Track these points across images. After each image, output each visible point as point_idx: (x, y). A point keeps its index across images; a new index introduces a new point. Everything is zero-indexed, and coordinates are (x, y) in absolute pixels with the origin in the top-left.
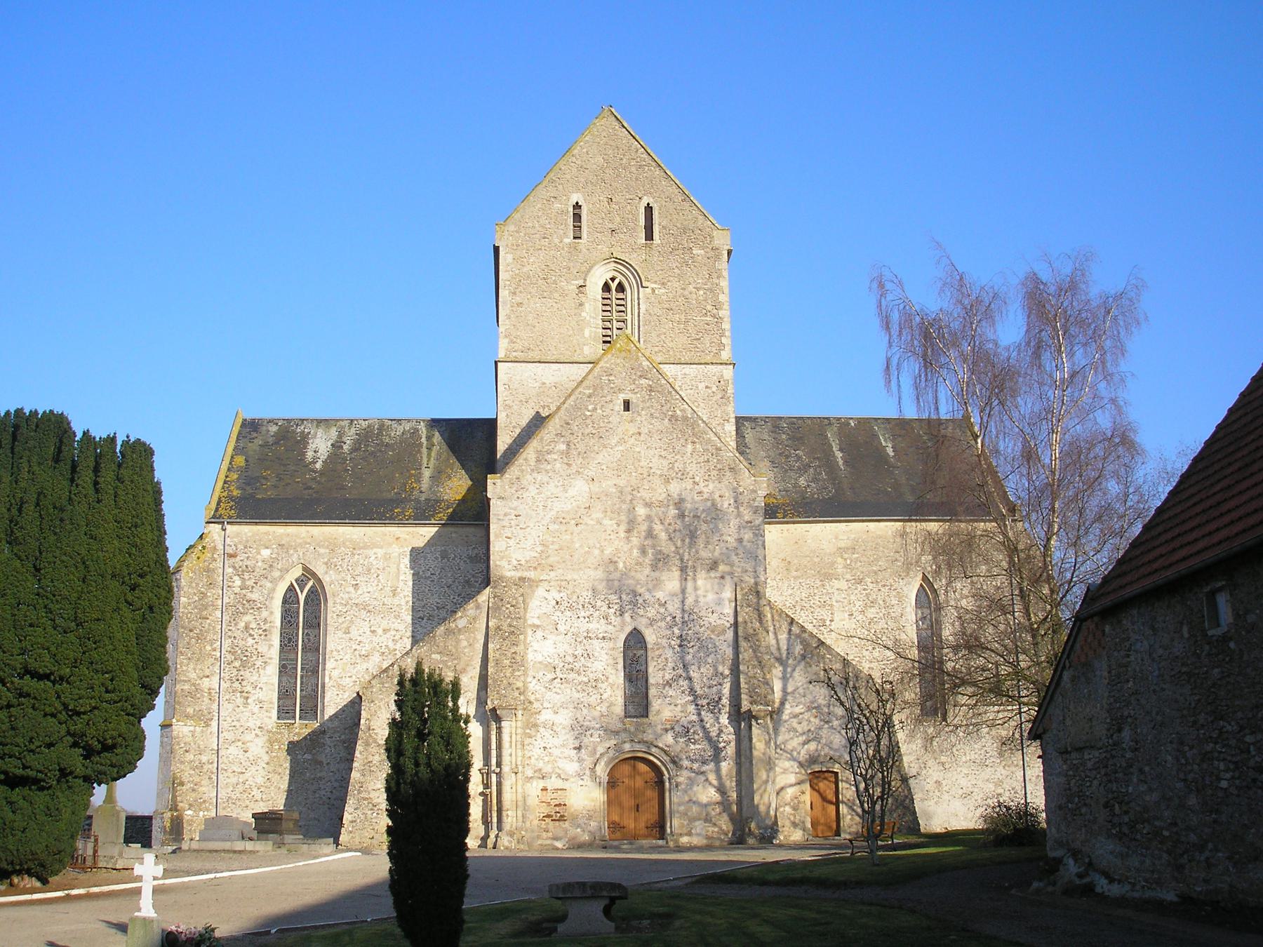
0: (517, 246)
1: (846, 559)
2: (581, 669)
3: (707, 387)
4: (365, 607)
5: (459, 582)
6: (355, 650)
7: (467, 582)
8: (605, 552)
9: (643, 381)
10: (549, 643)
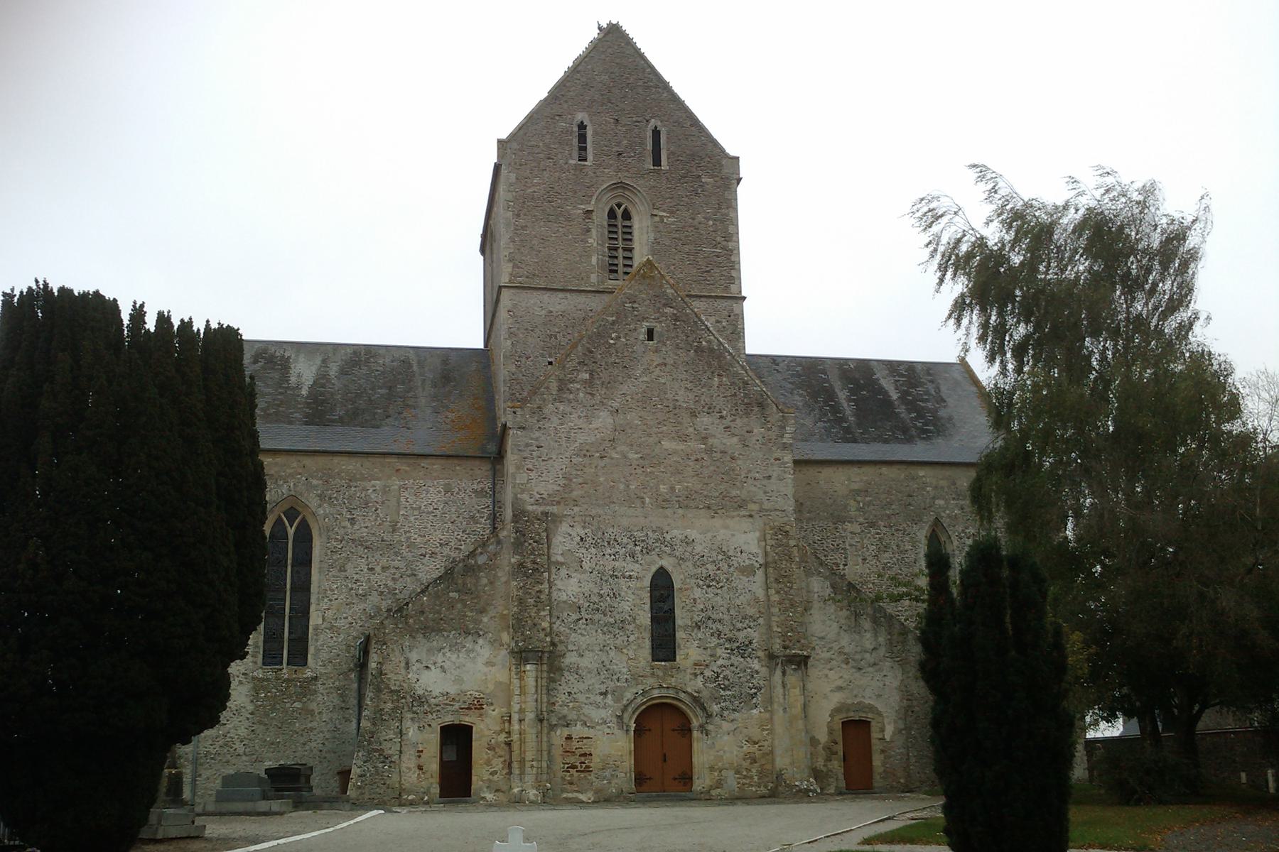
0: (521, 165)
1: (858, 502)
2: (607, 610)
3: (717, 322)
4: (361, 542)
5: (463, 518)
6: (352, 589)
7: (472, 517)
8: (631, 487)
9: (667, 310)
10: (574, 581)
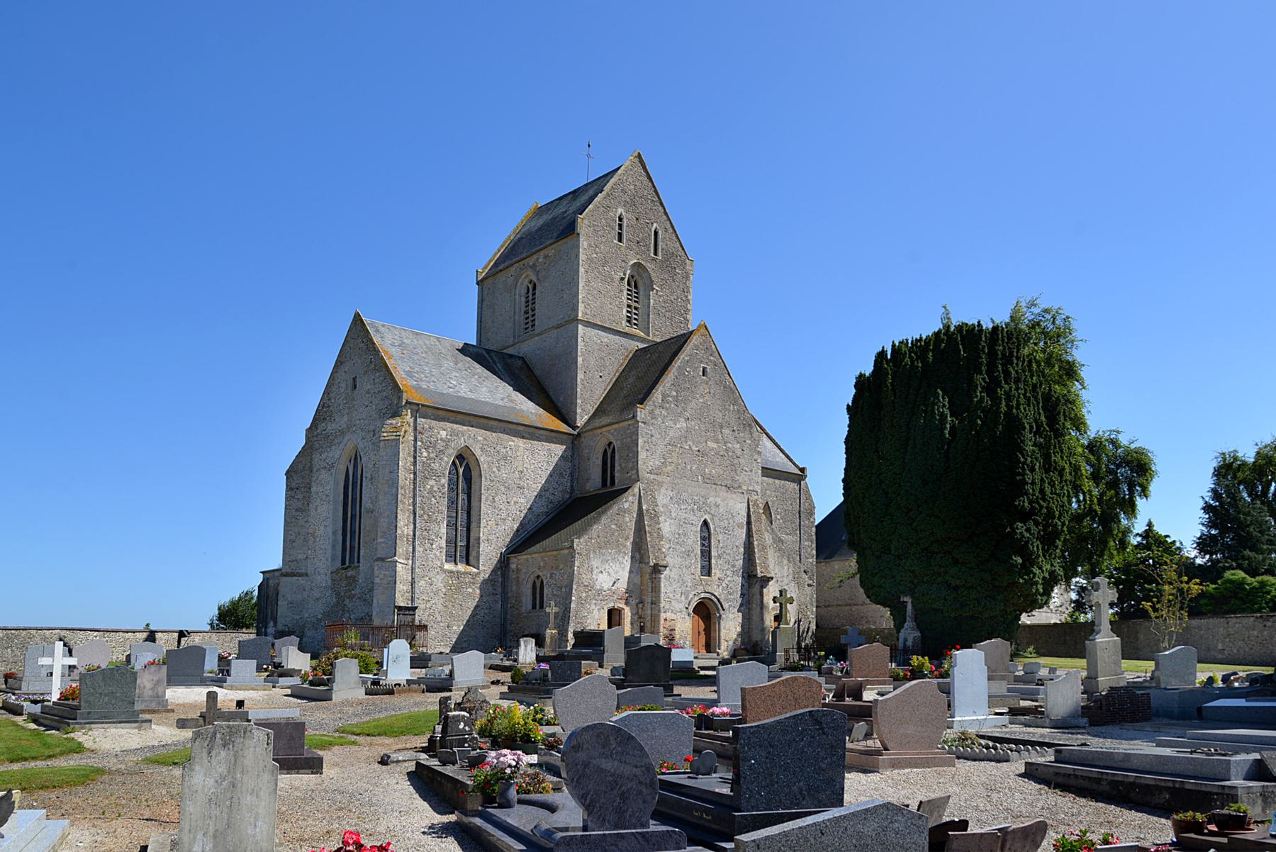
6: (498, 515)
7: (561, 474)
9: (712, 358)
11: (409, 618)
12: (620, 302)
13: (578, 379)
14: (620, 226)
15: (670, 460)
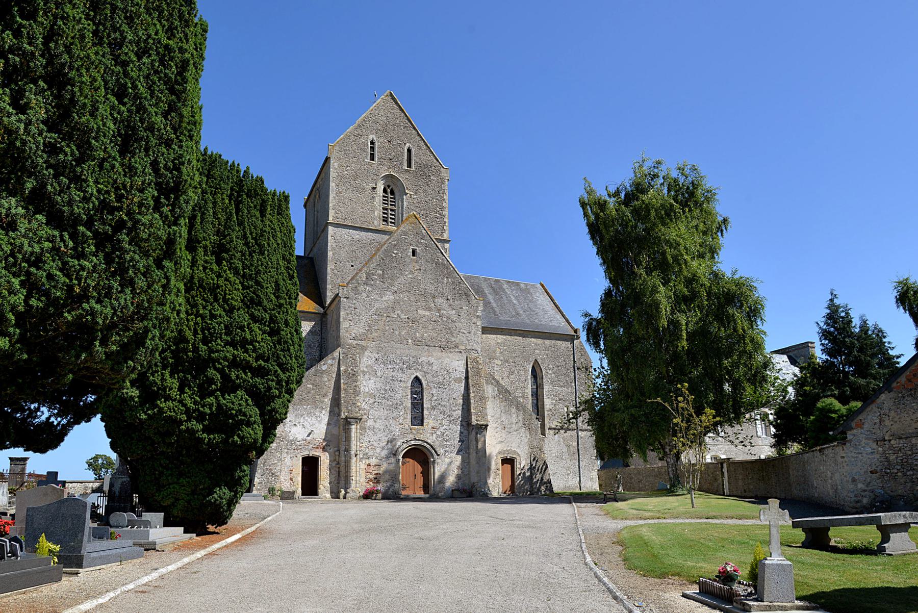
9: (422, 241)
11: (20, 467)
12: (372, 206)
13: (328, 268)
14: (372, 149)
15: (376, 328)
